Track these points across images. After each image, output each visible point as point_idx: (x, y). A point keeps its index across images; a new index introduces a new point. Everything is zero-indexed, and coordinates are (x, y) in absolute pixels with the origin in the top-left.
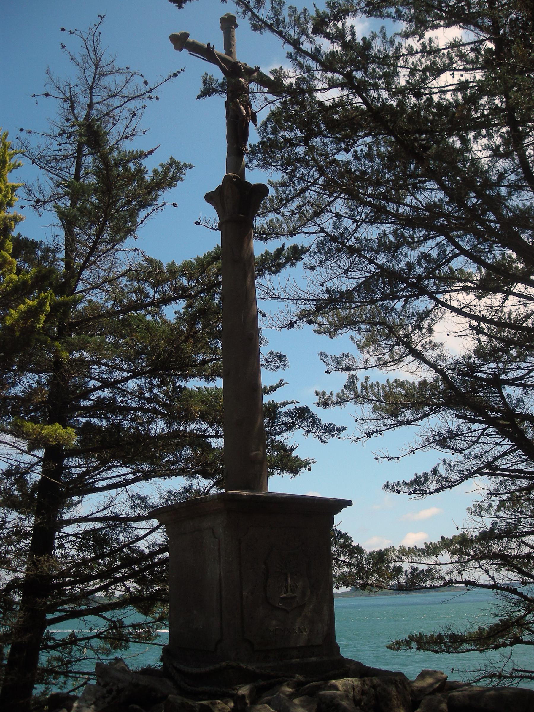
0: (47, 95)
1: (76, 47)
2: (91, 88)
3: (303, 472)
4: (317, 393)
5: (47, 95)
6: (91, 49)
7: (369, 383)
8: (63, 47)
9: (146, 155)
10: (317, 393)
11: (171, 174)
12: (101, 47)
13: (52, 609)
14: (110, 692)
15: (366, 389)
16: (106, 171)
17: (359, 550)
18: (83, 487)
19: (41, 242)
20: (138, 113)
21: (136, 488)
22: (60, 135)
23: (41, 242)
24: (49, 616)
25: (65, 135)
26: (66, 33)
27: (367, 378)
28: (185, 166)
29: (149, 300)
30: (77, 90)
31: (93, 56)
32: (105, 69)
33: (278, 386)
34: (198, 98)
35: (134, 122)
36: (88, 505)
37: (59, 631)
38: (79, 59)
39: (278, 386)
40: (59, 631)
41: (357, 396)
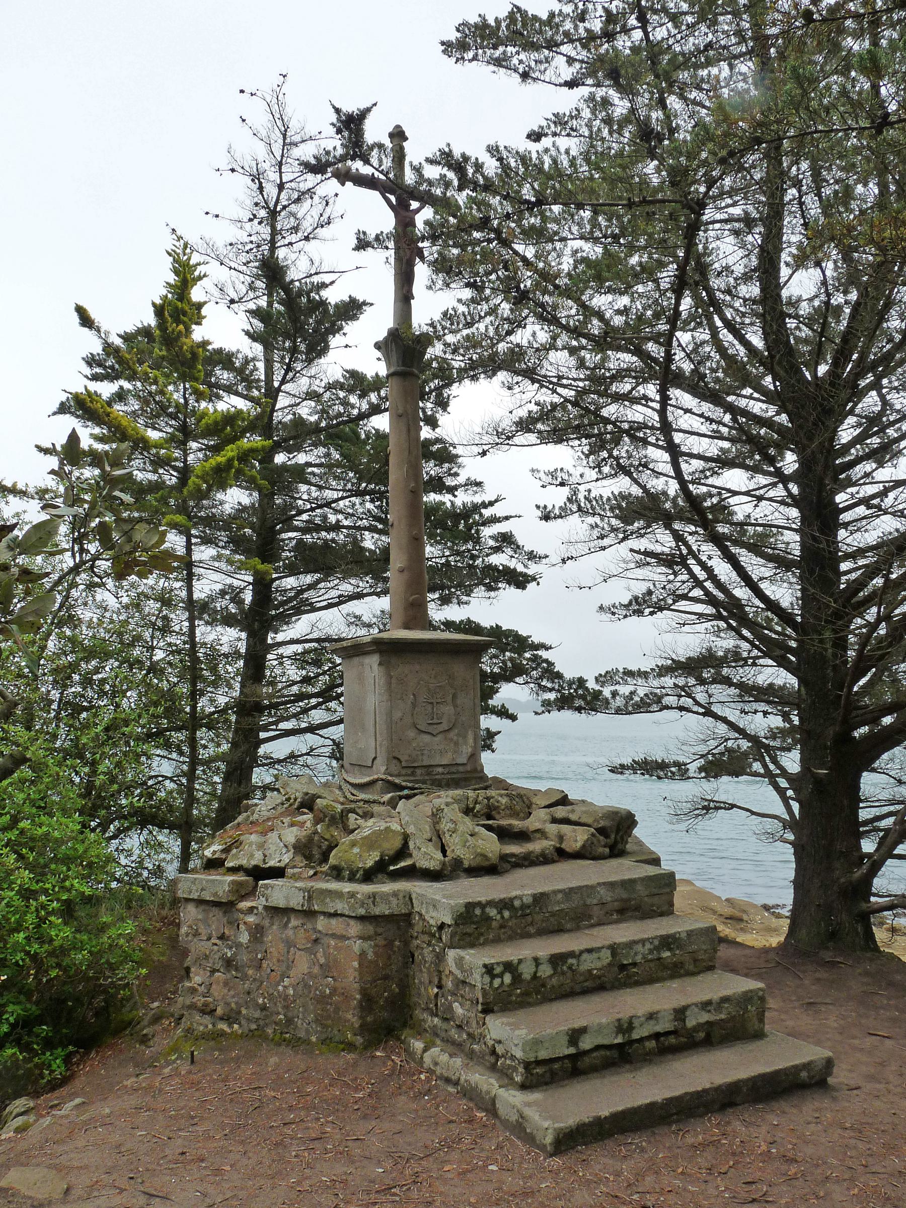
0: (233, 170)
1: (260, 118)
2: (280, 164)
3: (531, 586)
4: (538, 507)
5: (233, 170)
6: (277, 116)
7: (593, 495)
8: (244, 120)
9: (327, 286)
10: (538, 507)
11: (352, 309)
12: (288, 111)
13: (265, 728)
14: (288, 800)
15: (590, 502)
16: (291, 301)
17: (559, 676)
18: (301, 605)
19: (238, 351)
20: (331, 201)
21: (354, 607)
22: (251, 220)
23: (238, 351)
24: (263, 735)
25: (256, 221)
26: (246, 95)
27: (589, 491)
28: (365, 303)
29: (355, 412)
30: (266, 166)
31: (279, 123)
32: (297, 138)
33: (496, 501)
34: (456, 48)
35: (328, 209)
36: (301, 626)
37: (278, 749)
38: (263, 133)
39: (496, 501)
40: (278, 749)
41: (580, 509)
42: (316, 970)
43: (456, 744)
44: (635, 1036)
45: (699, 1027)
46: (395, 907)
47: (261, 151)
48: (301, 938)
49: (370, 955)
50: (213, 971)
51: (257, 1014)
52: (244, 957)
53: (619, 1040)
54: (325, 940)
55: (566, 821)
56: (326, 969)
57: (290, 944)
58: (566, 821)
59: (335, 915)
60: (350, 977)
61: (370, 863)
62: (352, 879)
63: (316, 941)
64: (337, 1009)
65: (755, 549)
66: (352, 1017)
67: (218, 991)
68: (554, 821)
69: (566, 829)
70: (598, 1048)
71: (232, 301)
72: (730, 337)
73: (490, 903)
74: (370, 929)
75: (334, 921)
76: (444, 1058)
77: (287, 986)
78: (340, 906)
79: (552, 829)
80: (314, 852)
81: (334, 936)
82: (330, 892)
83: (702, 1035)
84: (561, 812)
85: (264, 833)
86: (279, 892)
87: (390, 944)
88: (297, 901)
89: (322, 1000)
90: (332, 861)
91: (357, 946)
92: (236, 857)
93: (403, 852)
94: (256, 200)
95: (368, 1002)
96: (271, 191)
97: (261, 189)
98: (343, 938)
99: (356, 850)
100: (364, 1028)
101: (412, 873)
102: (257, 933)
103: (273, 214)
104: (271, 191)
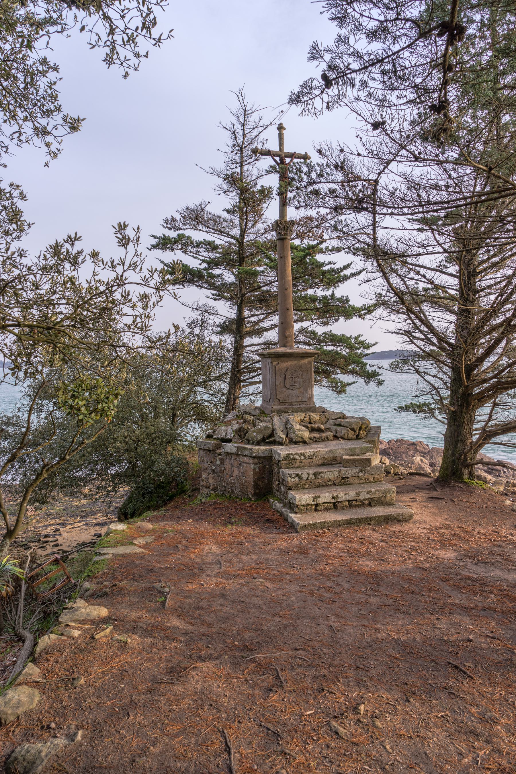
42: (240, 474)
43: (303, 393)
44: (339, 500)
45: (366, 499)
46: (267, 454)
47: (235, 122)
48: (236, 463)
49: (257, 470)
50: (209, 474)
51: (223, 489)
52: (218, 469)
53: (333, 501)
54: (243, 464)
55: (340, 425)
56: (243, 474)
57: (232, 465)
58: (340, 425)
59: (245, 456)
60: (250, 477)
61: (259, 438)
62: (253, 444)
63: (240, 464)
64: (247, 488)
65: (508, 282)
66: (251, 490)
67: (211, 481)
68: (335, 425)
69: (339, 428)
70: (324, 503)
71: (225, 192)
72: (435, 208)
73: (296, 454)
74: (256, 461)
75: (245, 458)
76: (278, 504)
77: (231, 480)
78: (247, 453)
79: (334, 428)
80: (241, 433)
81: (246, 463)
82: (244, 448)
83: (367, 502)
84: (338, 421)
85: (227, 426)
86: (230, 447)
87: (264, 467)
88: (234, 451)
89: (242, 484)
90: (246, 437)
91: (252, 466)
92: (217, 434)
93: (272, 435)
94: (233, 143)
95: (256, 486)
96: (240, 138)
97: (236, 138)
98: (248, 463)
99: (254, 434)
100: (255, 495)
101: (274, 443)
102: (222, 461)
103: (242, 150)
104: (240, 138)
